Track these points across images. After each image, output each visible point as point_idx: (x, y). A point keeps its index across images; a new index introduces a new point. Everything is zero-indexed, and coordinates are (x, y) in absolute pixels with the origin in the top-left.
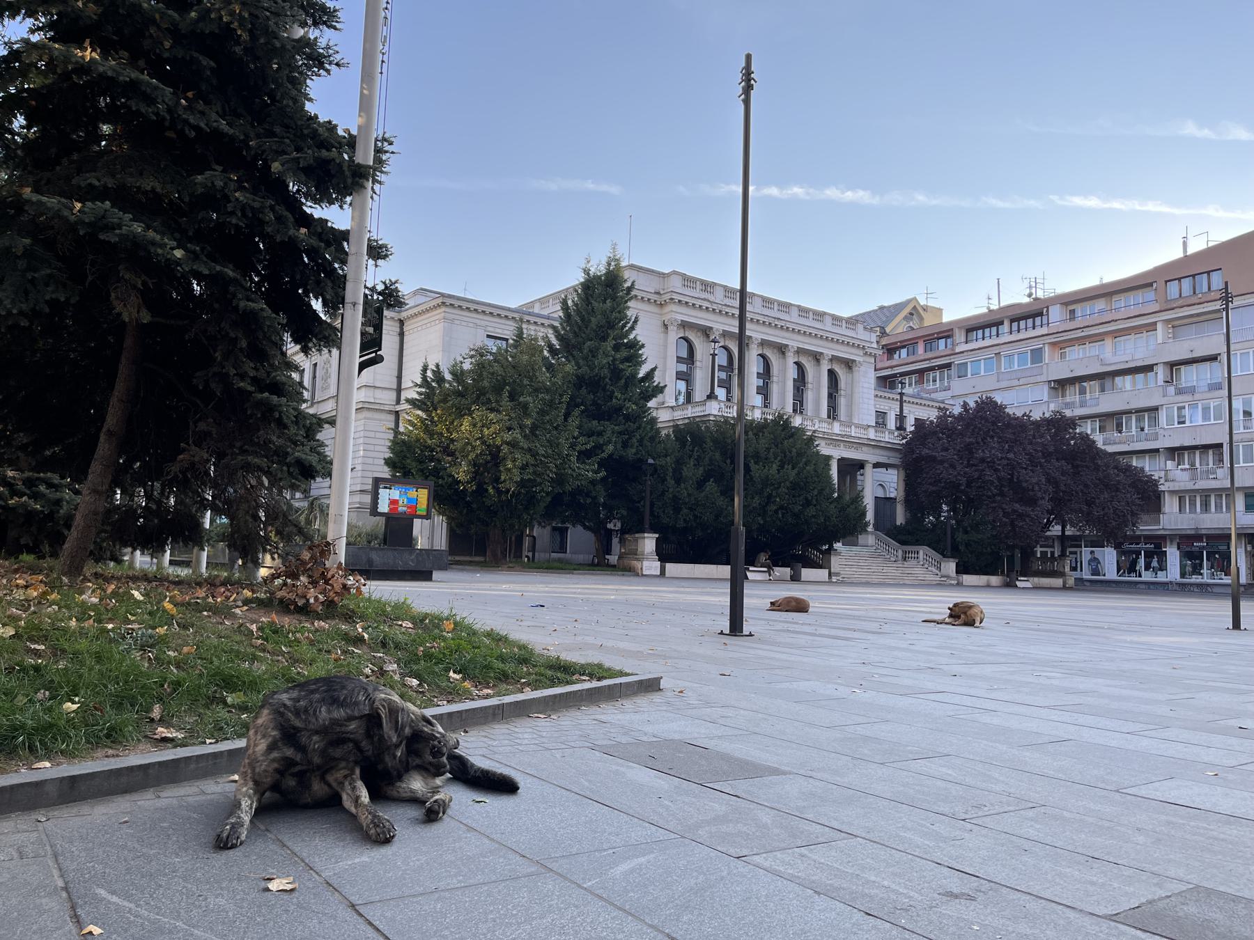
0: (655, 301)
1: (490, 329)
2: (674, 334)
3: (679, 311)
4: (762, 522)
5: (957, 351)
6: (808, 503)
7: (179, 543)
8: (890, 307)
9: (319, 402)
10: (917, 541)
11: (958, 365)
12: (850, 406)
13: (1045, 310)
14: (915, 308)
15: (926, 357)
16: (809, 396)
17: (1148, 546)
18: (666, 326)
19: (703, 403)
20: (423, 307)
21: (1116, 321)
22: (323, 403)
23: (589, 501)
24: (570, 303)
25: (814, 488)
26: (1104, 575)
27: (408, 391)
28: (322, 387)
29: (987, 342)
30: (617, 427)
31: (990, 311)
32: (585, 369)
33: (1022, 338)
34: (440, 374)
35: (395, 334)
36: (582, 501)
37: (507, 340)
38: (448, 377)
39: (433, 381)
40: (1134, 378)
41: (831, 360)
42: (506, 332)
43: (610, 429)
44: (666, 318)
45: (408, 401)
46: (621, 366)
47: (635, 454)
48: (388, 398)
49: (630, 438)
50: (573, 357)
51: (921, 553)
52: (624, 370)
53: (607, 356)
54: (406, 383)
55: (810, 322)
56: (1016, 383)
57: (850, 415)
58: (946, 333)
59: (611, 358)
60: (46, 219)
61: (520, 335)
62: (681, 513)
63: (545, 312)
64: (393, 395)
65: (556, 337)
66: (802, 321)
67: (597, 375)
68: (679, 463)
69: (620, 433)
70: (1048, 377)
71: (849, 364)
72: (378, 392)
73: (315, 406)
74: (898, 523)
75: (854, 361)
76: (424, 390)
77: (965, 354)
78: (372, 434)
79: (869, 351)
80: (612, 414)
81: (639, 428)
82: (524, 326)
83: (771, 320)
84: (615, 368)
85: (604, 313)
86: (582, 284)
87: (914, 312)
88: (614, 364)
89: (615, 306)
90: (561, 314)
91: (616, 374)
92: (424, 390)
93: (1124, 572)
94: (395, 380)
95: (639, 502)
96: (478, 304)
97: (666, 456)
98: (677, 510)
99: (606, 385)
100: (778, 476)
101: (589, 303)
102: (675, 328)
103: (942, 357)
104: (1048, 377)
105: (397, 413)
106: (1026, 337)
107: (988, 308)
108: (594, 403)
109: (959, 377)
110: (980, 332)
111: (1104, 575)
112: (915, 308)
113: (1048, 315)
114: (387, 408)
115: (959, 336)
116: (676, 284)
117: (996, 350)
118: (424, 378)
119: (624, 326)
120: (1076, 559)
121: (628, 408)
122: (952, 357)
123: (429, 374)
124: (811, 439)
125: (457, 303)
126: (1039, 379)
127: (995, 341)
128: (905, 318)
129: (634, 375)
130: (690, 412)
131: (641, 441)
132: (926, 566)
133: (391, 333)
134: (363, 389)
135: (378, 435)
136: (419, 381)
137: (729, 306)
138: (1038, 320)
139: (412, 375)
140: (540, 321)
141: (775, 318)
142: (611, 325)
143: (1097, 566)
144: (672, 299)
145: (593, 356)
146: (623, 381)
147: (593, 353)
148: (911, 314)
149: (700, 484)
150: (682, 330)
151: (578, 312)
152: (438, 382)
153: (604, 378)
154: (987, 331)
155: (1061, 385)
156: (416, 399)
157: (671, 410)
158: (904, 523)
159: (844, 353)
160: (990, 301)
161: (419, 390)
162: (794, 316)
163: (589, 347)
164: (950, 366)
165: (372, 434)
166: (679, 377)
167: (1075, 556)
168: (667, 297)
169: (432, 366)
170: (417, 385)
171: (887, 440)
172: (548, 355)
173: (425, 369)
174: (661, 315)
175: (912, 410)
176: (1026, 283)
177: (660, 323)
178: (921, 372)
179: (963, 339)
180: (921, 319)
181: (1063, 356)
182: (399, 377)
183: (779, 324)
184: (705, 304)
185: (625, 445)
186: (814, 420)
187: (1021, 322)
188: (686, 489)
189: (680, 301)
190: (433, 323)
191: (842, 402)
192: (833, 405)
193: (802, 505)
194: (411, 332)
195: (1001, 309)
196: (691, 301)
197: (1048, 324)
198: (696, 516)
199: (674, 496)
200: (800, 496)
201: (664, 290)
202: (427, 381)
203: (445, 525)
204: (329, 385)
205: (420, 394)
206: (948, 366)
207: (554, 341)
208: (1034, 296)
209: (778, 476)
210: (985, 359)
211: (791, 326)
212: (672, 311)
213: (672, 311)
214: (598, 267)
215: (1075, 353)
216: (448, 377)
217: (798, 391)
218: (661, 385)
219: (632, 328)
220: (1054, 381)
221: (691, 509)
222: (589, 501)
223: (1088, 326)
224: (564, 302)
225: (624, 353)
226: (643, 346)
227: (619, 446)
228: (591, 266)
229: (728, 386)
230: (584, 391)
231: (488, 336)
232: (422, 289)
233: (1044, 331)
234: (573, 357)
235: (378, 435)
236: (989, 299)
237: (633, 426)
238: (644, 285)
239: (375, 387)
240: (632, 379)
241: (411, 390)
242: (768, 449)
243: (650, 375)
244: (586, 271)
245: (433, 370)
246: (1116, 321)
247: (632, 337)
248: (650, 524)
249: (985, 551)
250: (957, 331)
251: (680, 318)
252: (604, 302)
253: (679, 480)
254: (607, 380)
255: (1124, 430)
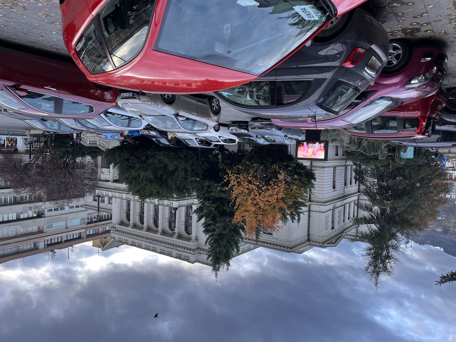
0: (201, 250)
1: (271, 238)
2: (193, 235)
3: (191, 246)
4: (148, 152)
5: (84, 229)
6: (128, 160)
7: (387, 151)
8: (114, 247)
9: (342, 206)
10: (90, 149)
11: (84, 224)
12: (121, 206)
13: (46, 247)
14: (103, 246)
15: (98, 227)
16: (152, 213)
17: (3, 150)
18: (197, 239)
19: (180, 206)
20: (300, 247)
21: (15, 242)
22: (341, 205)
23: (226, 161)
24: (235, 250)
25: (124, 166)
26: (22, 138)
27: (306, 210)
28: (341, 212)
29: (71, 233)
30: (213, 194)
31: (71, 246)
32: (228, 220)
33: (56, 235)
34: (292, 218)
35: (311, 235)
36: (229, 161)
37: (264, 233)
38: (288, 217)
39: (295, 215)
40: (8, 219)
41: (129, 225)
42: (264, 236)
43: (215, 194)
44: (196, 243)
45: (306, 206)
46: (211, 222)
47: (205, 183)
48: (314, 207)
49: (207, 190)
50: (233, 226)
51: (88, 143)
52: (210, 220)
53: (218, 227)
54: (306, 214)
55: (137, 241)
56: (59, 217)
57: (121, 202)
58: (89, 237)
59: (216, 225)
60: (16, 158)
61: (257, 235)
62: (184, 155)
63: (248, 245)
64: (312, 209)
65: (241, 235)
66: (141, 242)
67: (223, 217)
68: (186, 179)
69: (212, 192)
70: (45, 219)
71: (122, 223)
72: (318, 210)
73: (344, 204)
74: (100, 157)
75: (120, 225)
76: (299, 210)
77: (81, 228)
78: (320, 192)
79: (114, 229)
80: (216, 200)
81: (204, 194)
82: (255, 239)
83: (153, 242)
84: (214, 221)
85: (220, 246)
86: (230, 259)
87: (104, 245)
88: (215, 223)
89: (215, 249)
90: (239, 245)
91: (214, 219)
92: (299, 210)
93: (14, 139)
94: (311, 215)
95: (203, 160)
96: (276, 249)
97: (191, 181)
98: (186, 156)
99: (218, 213)
100: (140, 172)
101: (227, 250)
102: (192, 239)
103: (91, 227)
104: (45, 219)
105: (310, 201)
106: (55, 235)
107: (72, 247)
108: (224, 205)
109: (84, 219)
110: (75, 237)
111: (22, 138)
112: (103, 246)
113: (45, 245)
114: (314, 203)
115: (84, 235)
116: (192, 257)
117: (67, 230)
118: (299, 216)
119: (211, 240)
120: (35, 145)
121: (209, 203)
122: (86, 227)
123: (297, 218)
124: (130, 190)
125: (285, 249)
126: (49, 218)
127: (68, 234)
128: (107, 242)
129: (206, 218)
130: (185, 202)
131: (203, 188)
132: (86, 138)
133: (313, 235)
134: (324, 211)
135: (318, 192)
136: (301, 215)
137: (170, 248)
138: (49, 243)
139: (304, 217)
140: (250, 241)
141: (151, 243)
142: (216, 241)
143: (26, 142)
144: (194, 251)
145: (224, 226)
146: (211, 215)
147: (225, 229)
148: (105, 244)
149: (176, 169)
150: (190, 238)
151: (231, 246)
152: (293, 214)
153: (219, 216)
154: (72, 238)
155: (40, 215)
156: (302, 206)
157: (194, 203)
158: (98, 157)
159: (123, 228)
160: (72, 250)
161: (301, 211)
162: (144, 244)
163: (226, 230)
164: (87, 223)
165: (320, 192)
166: (191, 218)
167: (35, 146)
168: (196, 252)
169: (296, 221)
170: (302, 213)
171: (104, 192)
172: (245, 227)
173: (299, 220)
174: (198, 244)
175: (105, 206)
176: (56, 257)
177: (199, 241)
178: (100, 220)
179: (82, 234)
180: (101, 242)
181: (39, 228)
182: (309, 216)
183: (149, 241)
184: (180, 249)
185: (209, 187)
186: (135, 199)
187: (57, 242)
188: (182, 166)
189: (190, 250)
190: (295, 240)
191: (125, 208)
192: (156, 211)
193: (130, 159)
194: (305, 236)
195: (68, 247)
196: (186, 250)
197: (44, 241)
198: (177, 154)
199: (187, 163)
200: (131, 164)
201: (198, 255)
202: (298, 215)
203: (289, 151)
204: (338, 213)
205: (301, 209)
206: (88, 223)
207: (241, 232)
208: (53, 252)
209: (140, 172)
210: (79, 225)
211: (144, 240)
212: (194, 246)
213: (194, 246)
214: (223, 268)
215: (35, 229)
216: (288, 217)
217: (157, 215)
218: (195, 214)
219: (208, 239)
220: (42, 217)
221: (180, 157)
222: (226, 161)
223: (27, 240)
224: (238, 250)
225: (210, 228)
226: (203, 231)
227: (212, 186)
228: (226, 267)
229: (171, 214)
230: (228, 211)
231: (272, 235)
232: (300, 253)
233: (46, 238)
234: (233, 226)
235: (318, 192)
236: (72, 251)
237: (206, 195)
238: (204, 257)
239: (320, 212)
240: (207, 216)
241: (304, 211)
242: (146, 185)
243: (200, 219)
244: (228, 264)
245: (295, 219)
246: (15, 242)
247: (208, 236)
248: (198, 151)
249: (59, 144)
250: (85, 237)
251: (190, 243)
252: (220, 251)
253: (186, 170)
254: (218, 216)
255: (13, 197)
